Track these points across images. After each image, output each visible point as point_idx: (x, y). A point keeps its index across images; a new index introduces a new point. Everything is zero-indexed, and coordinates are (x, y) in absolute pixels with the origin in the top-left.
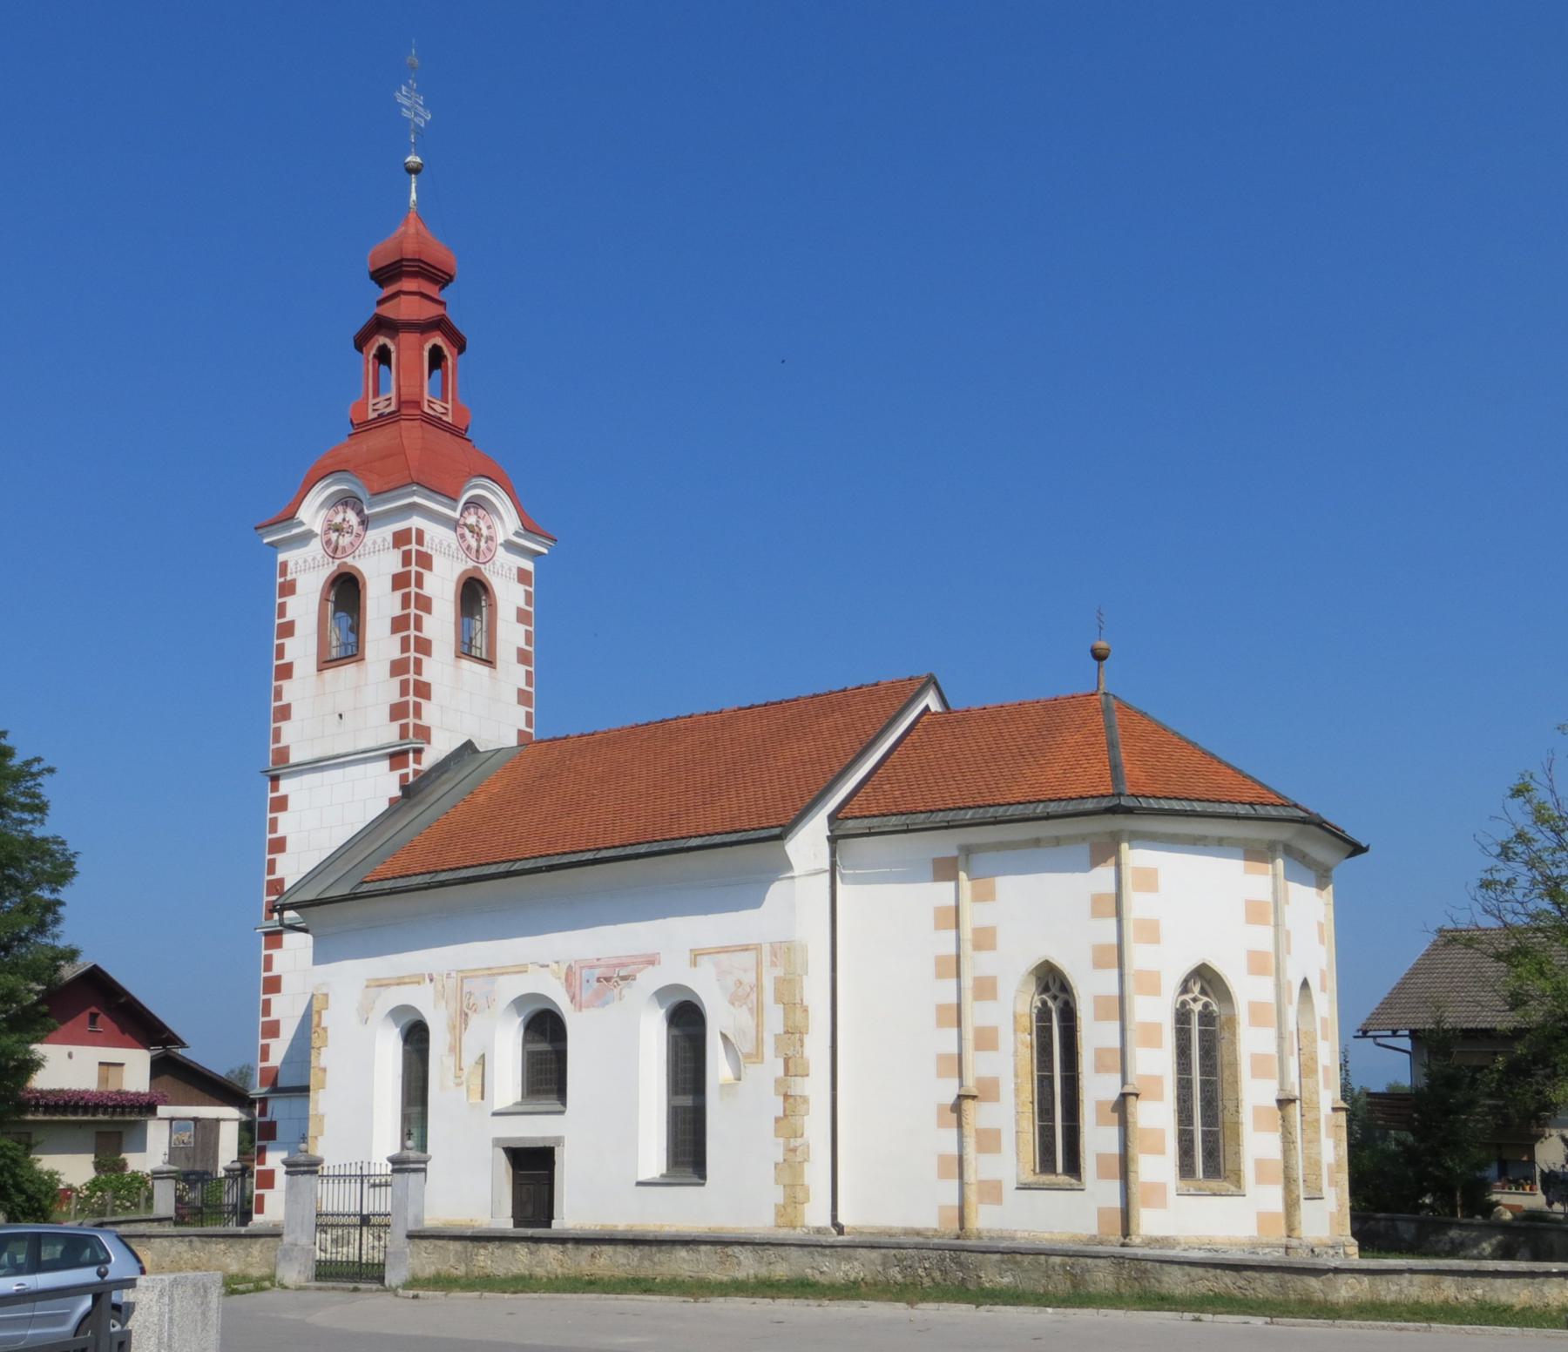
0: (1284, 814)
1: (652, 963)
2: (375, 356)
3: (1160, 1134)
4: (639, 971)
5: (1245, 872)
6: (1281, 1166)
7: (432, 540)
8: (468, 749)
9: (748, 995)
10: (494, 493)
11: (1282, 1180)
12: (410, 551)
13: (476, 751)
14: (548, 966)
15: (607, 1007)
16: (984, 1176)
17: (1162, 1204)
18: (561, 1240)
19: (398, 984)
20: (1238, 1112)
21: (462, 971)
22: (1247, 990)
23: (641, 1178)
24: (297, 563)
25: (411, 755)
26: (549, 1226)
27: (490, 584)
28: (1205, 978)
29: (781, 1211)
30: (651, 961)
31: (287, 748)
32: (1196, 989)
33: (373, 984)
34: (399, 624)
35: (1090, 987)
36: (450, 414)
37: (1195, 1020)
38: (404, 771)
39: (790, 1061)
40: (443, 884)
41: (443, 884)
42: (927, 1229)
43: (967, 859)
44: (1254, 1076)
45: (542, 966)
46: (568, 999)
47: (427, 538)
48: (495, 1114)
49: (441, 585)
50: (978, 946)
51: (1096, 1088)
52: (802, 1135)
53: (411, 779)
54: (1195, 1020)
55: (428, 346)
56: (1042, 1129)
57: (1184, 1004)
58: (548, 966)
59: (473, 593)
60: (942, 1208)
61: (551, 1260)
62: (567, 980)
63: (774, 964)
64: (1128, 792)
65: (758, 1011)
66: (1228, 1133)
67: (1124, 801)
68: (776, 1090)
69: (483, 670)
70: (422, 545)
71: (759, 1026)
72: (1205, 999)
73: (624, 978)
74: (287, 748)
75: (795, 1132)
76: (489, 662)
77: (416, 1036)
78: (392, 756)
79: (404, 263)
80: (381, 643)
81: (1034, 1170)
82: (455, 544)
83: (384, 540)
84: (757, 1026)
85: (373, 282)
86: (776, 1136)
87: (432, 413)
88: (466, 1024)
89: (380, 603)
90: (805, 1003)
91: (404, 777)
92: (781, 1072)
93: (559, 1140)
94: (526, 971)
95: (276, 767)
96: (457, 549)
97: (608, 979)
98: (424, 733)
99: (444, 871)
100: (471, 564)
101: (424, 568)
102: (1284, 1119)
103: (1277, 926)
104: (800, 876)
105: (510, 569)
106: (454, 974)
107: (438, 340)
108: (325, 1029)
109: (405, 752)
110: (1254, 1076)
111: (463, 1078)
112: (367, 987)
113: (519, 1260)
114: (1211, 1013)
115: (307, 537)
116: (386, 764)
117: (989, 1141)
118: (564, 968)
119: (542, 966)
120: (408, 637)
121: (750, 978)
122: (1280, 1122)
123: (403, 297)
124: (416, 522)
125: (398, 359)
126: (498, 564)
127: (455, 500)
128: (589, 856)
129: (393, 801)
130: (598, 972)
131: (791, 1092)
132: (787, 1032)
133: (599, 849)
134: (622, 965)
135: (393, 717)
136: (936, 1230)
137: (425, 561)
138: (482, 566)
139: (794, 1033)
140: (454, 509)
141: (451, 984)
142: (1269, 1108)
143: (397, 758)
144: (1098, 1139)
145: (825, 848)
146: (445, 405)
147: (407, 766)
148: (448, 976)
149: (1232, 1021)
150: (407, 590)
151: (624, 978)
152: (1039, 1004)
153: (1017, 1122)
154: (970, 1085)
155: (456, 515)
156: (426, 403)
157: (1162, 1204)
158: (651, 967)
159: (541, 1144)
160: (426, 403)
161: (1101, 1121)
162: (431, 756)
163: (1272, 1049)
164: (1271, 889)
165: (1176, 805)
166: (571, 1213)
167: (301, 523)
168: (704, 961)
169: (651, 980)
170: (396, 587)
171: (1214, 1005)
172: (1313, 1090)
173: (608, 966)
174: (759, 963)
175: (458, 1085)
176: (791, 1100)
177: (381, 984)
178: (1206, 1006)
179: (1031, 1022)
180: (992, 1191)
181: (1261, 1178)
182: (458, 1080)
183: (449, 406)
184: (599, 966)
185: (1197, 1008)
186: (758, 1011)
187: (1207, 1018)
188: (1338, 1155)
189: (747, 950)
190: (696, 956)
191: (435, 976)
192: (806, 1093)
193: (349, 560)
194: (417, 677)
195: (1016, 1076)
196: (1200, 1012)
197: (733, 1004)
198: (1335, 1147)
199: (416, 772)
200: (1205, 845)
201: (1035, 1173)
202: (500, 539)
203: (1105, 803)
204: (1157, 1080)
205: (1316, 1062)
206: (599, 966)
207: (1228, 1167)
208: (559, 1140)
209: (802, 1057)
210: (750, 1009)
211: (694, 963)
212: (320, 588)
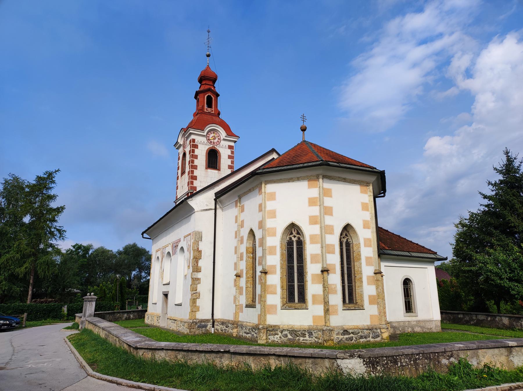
3: (275, 286)
17: (275, 313)
23: (176, 303)
36: (213, 111)
37: (295, 244)
44: (367, 265)
47: (196, 141)
49: (202, 152)
52: (196, 290)
54: (295, 244)
55: (206, 96)
72: (298, 236)
79: (202, 78)
95: (266, 212)
96: (207, 143)
100: (211, 146)
105: (226, 146)
110: (367, 265)
114: (301, 241)
124: (193, 137)
126: (221, 145)
136: (232, 321)
138: (216, 146)
140: (204, 133)
146: (212, 109)
149: (305, 243)
157: (275, 313)
163: (319, 252)
171: (301, 238)
172: (359, 266)
181: (371, 302)
188: (378, 292)
198: (377, 289)
202: (222, 139)
204: (274, 267)
205: (360, 256)
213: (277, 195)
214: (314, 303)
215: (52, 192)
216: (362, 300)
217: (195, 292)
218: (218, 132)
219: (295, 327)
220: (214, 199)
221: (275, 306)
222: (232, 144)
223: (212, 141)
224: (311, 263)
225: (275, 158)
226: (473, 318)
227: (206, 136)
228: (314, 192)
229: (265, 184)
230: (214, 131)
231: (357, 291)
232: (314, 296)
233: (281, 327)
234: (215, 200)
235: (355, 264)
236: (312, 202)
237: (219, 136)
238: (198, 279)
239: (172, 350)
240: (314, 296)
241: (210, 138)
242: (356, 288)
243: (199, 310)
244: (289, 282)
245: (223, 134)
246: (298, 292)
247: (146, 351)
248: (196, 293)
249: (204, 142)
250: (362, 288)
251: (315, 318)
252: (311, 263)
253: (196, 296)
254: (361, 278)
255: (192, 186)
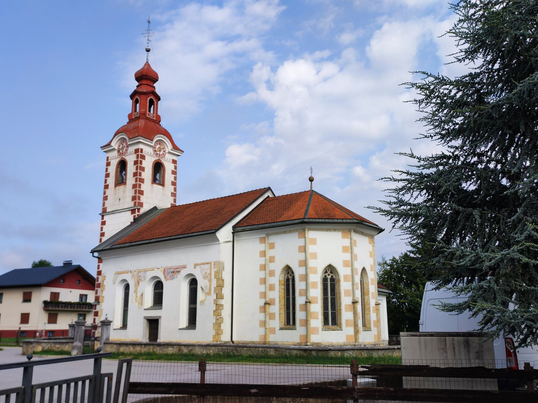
0: (351, 221)
1: (185, 268)
2: (135, 101)
4: (182, 270)
5: (342, 238)
6: (353, 322)
7: (145, 151)
8: (155, 208)
9: (208, 276)
10: (165, 139)
11: (353, 326)
12: (139, 154)
13: (157, 209)
14: (159, 268)
15: (173, 280)
16: (271, 326)
17: (317, 333)
18: (159, 345)
19: (123, 273)
20: (340, 306)
21: (138, 270)
22: (343, 272)
23: (180, 328)
24: (111, 157)
25: (137, 210)
26: (156, 341)
27: (164, 164)
28: (331, 269)
29: (214, 337)
30: (184, 267)
31: (106, 208)
32: (329, 272)
33: (117, 273)
34: (135, 174)
35: (298, 272)
36: (155, 117)
37: (329, 280)
38: (134, 215)
39: (218, 295)
40: (132, 246)
41: (132, 246)
42: (256, 342)
43: (268, 238)
44: (345, 296)
45: (158, 269)
46: (164, 277)
47: (144, 151)
48: (145, 309)
49: (148, 164)
50: (270, 262)
51: (300, 300)
52: (221, 315)
53: (136, 217)
54: (329, 280)
55: (148, 99)
56: (287, 312)
57: (325, 276)
58: (159, 268)
59: (158, 167)
60: (260, 336)
61: (158, 350)
62: (164, 272)
63: (214, 268)
64: (307, 218)
65: (210, 281)
66: (338, 312)
67: (305, 220)
68: (214, 303)
69: (161, 187)
70: (142, 153)
71: (210, 285)
72: (332, 274)
73: (178, 272)
74: (106, 208)
75: (218, 314)
76: (163, 185)
77: (127, 287)
78: (132, 210)
80: (130, 180)
81: (285, 324)
82: (152, 153)
83: (132, 151)
84: (210, 285)
85: (136, 81)
86: (214, 316)
87: (149, 117)
88: (139, 284)
89: (131, 168)
90: (223, 278)
91: (134, 216)
92: (215, 298)
93: (160, 317)
94: (154, 270)
96: (153, 154)
97: (174, 272)
98: (141, 205)
99: (133, 242)
100: (157, 158)
101: (142, 159)
102: (354, 307)
103: (351, 253)
104: (222, 243)
105: (170, 160)
106: (136, 271)
107: (152, 97)
108: (104, 286)
109: (135, 209)
110: (345, 296)
111: (137, 300)
112: (115, 274)
113: (151, 349)
114: (334, 278)
115: (114, 149)
116: (130, 212)
117: (272, 316)
118: (163, 269)
119: (158, 269)
120: (137, 178)
121: (208, 272)
122: (353, 309)
123: (143, 85)
124: (141, 146)
125: (140, 102)
126: (166, 158)
127: (152, 140)
128: (168, 238)
129: (132, 223)
130: (172, 270)
131: (218, 303)
132: (217, 287)
133: (171, 236)
134: (177, 268)
135: (133, 200)
136: (259, 342)
137: (143, 157)
138: (161, 159)
139: (220, 286)
140: (152, 143)
141: (135, 273)
142: (349, 305)
143: (133, 211)
144: (300, 315)
145: (231, 235)
147: (135, 213)
148: (135, 271)
149: (339, 280)
150: (137, 165)
151: (178, 272)
152: (287, 277)
153: (280, 311)
154: (268, 300)
155: (153, 145)
156: (148, 114)
157: (317, 333)
158: (184, 269)
159: (155, 318)
160: (148, 114)
161: (301, 310)
162: (143, 210)
164: (350, 243)
165: (321, 220)
166: (163, 337)
167: (112, 146)
168: (197, 267)
169: (184, 272)
170: (135, 164)
173: (174, 268)
174: (211, 267)
175: (136, 301)
176: (218, 306)
177: (119, 273)
178: (332, 276)
179: (284, 282)
180: (273, 331)
182: (136, 300)
183: (155, 115)
184: (172, 269)
185: (329, 277)
186: (210, 281)
187: (332, 280)
189: (208, 264)
190: (196, 265)
191: (132, 271)
192: (222, 303)
193: (124, 157)
194: (139, 189)
195: (279, 298)
196: (330, 278)
197: (204, 279)
198: (377, 316)
199: (138, 215)
200: (330, 231)
201: (285, 325)
202: (167, 151)
203: (300, 221)
204: (316, 298)
205: (369, 291)
206: (172, 269)
207: (338, 322)
208: (160, 317)
209: (221, 293)
210: (208, 280)
211: (195, 268)
212: (116, 164)
213: (317, 240)
214: (347, 326)
215: (379, 267)
216: (370, 324)
217: (220, 317)
218: (164, 144)
219: (334, 343)
220: (232, 232)
221: (318, 328)
222: (175, 158)
223: (158, 153)
224: (345, 296)
225: (270, 196)
226: (394, 339)
227: (154, 147)
228: (346, 242)
229: (308, 231)
230: (160, 142)
231: (366, 317)
232: (347, 321)
233: (323, 343)
234: (233, 233)
235: (365, 298)
236: (345, 249)
237: (164, 148)
238: (222, 305)
239: (358, 350)
240: (347, 321)
241: (157, 150)
242: (366, 315)
243: (222, 334)
244: (324, 310)
245: (169, 147)
246: (331, 318)
247: (337, 351)
248: (221, 318)
249: (151, 153)
250: (370, 315)
251: (348, 337)
252: (345, 296)
253: (221, 320)
254: (370, 308)
255: (139, 201)
